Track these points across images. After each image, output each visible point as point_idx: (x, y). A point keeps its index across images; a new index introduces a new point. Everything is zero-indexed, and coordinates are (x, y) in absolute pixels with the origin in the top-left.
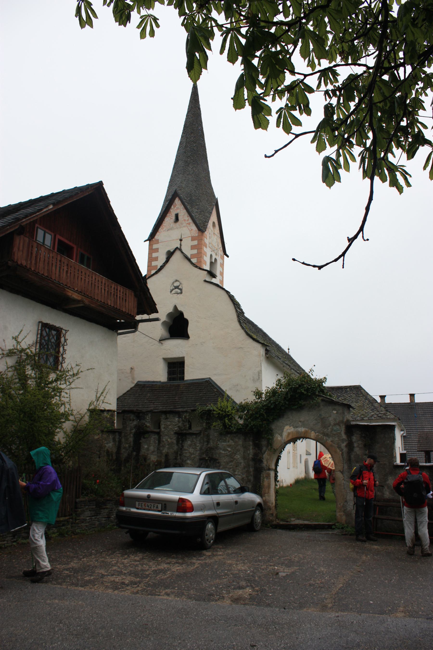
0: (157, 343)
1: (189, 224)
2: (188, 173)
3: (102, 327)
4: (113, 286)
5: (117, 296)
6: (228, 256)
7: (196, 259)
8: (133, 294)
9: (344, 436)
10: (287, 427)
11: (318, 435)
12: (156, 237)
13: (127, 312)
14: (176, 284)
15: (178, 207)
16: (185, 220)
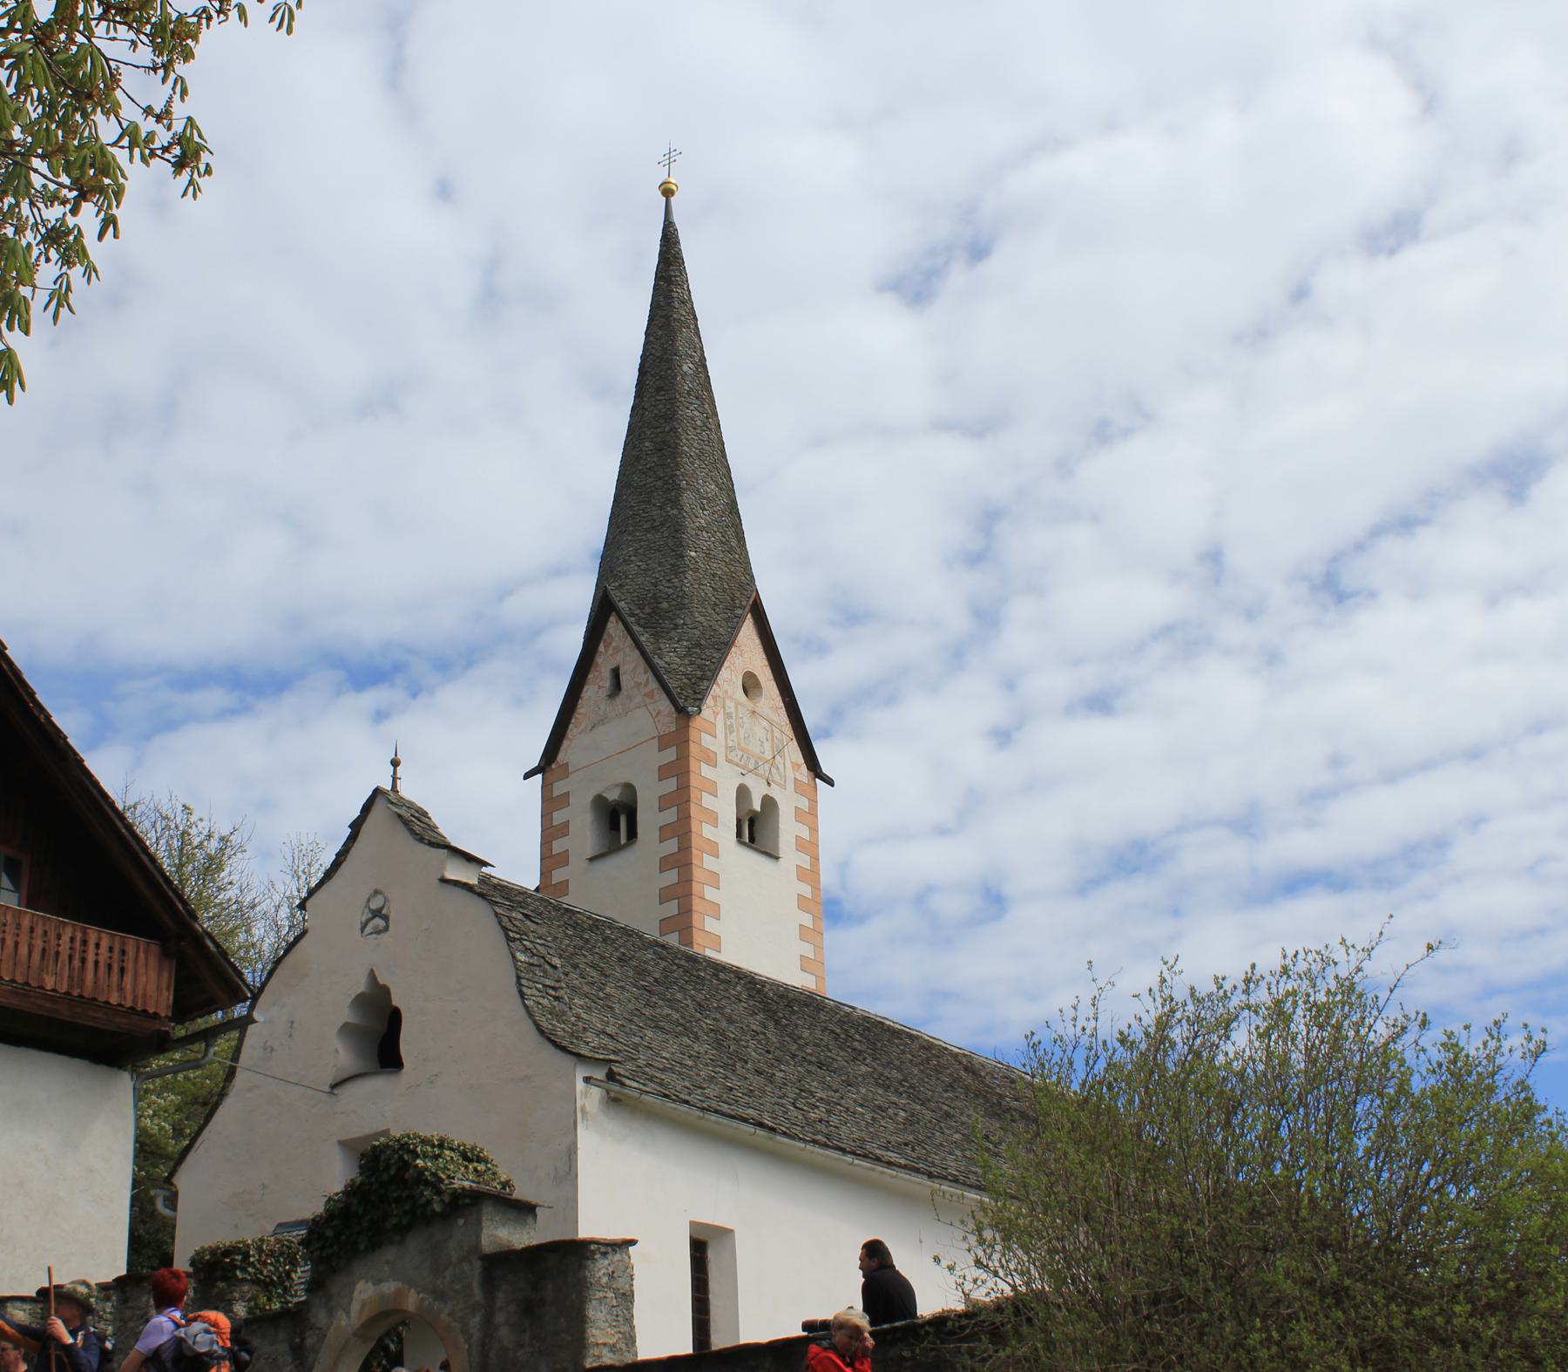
0: (326, 1097)
1: (650, 695)
2: (646, 526)
3: (86, 1063)
4: (68, 933)
5: (83, 961)
6: (830, 782)
7: (675, 809)
8: (155, 948)
9: (478, 1295)
10: (360, 1285)
11: (423, 1300)
12: (561, 757)
13: (129, 1004)
14: (375, 905)
15: (618, 650)
16: (638, 685)
